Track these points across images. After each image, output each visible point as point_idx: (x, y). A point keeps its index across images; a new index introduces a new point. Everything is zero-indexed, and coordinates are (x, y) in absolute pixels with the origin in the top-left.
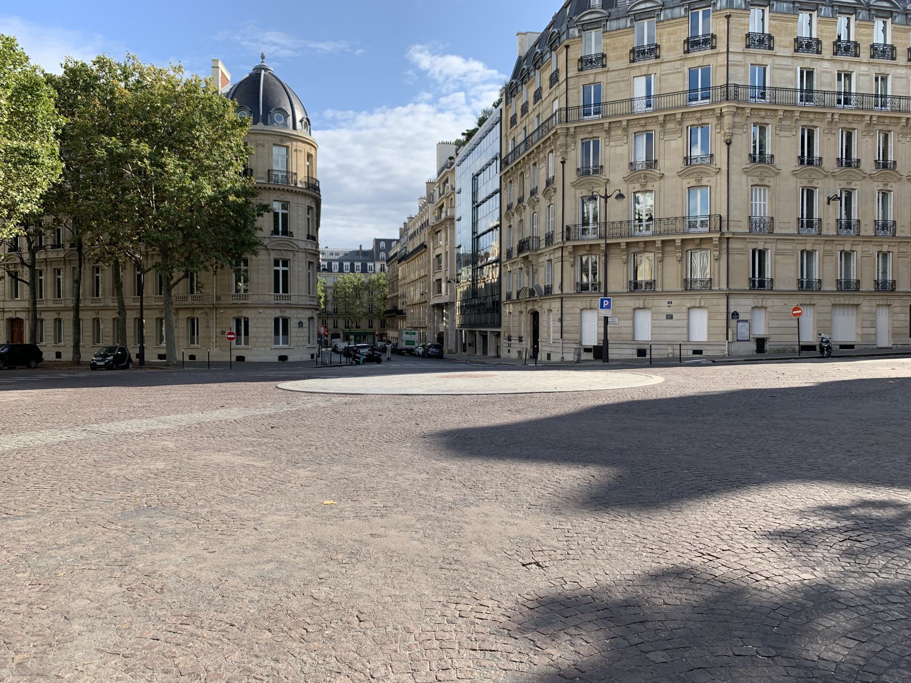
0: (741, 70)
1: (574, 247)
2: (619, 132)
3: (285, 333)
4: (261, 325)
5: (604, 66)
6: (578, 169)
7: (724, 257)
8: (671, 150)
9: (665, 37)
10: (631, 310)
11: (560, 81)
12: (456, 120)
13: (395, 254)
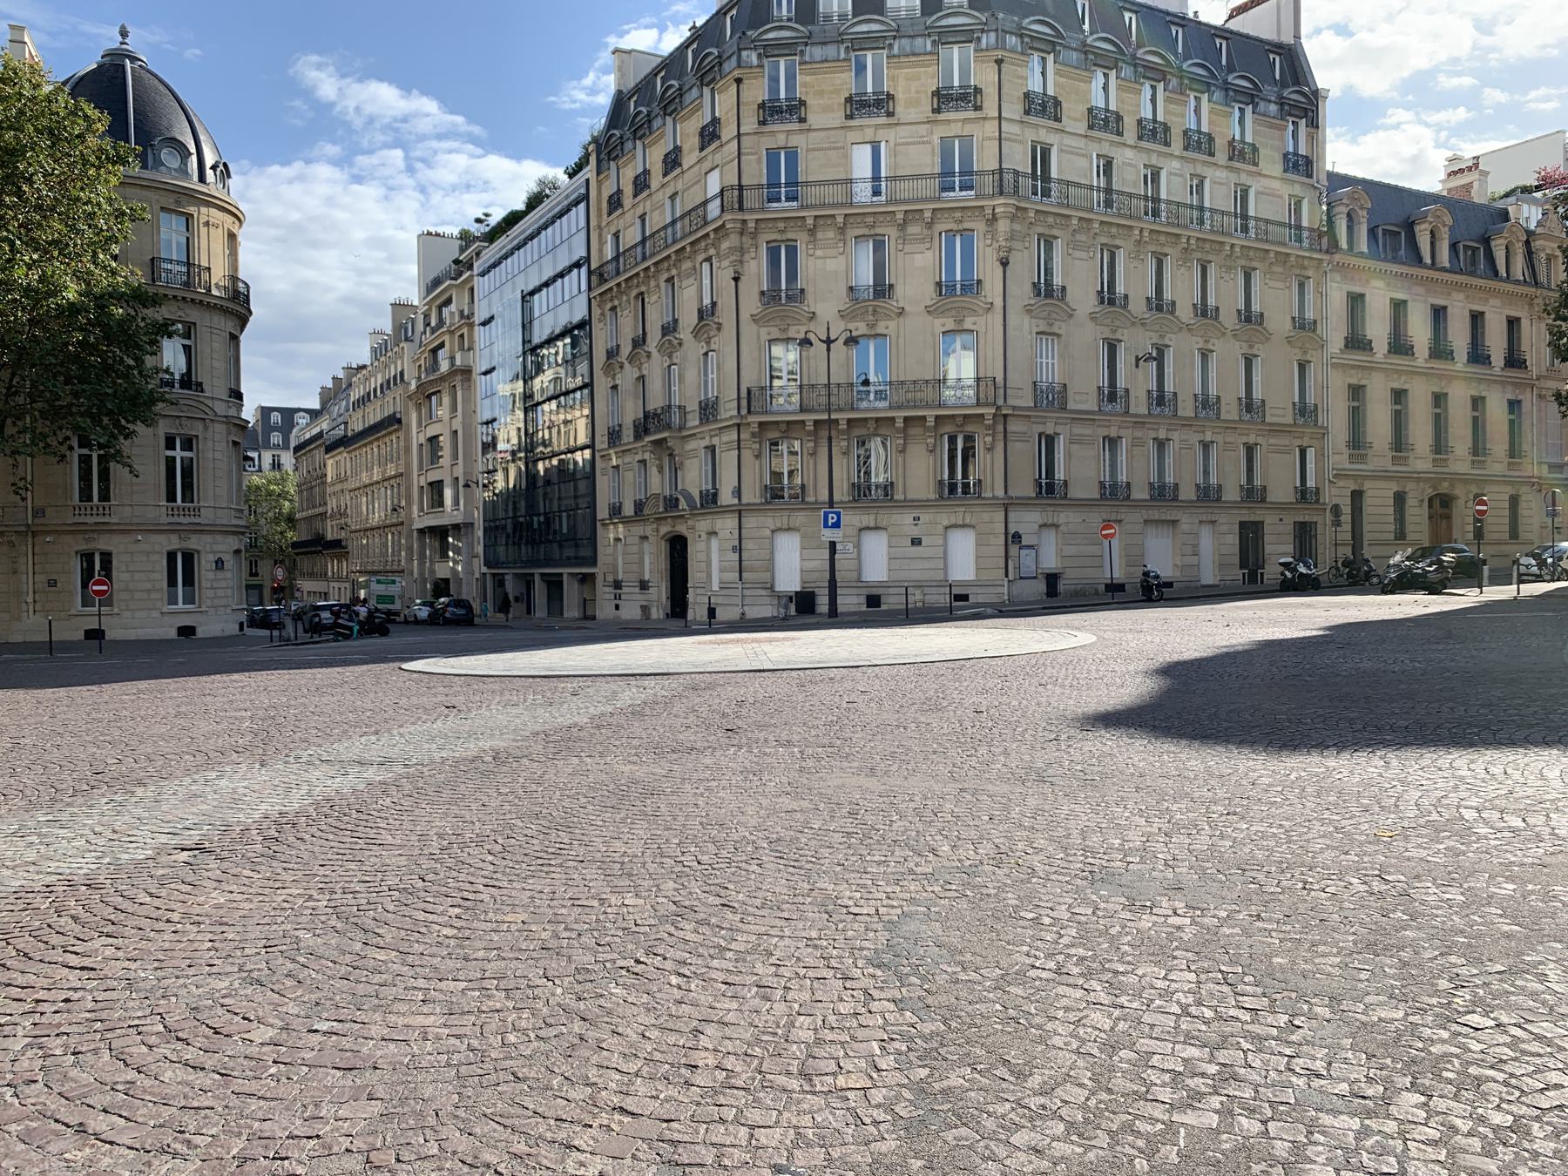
0: (1018, 148)
1: (761, 424)
2: (831, 234)
3: (189, 580)
4: (139, 567)
5: (802, 120)
6: (762, 293)
7: (1000, 446)
8: (917, 271)
9: (902, 83)
10: (855, 532)
11: (724, 138)
12: (386, 198)
13: (320, 435)
